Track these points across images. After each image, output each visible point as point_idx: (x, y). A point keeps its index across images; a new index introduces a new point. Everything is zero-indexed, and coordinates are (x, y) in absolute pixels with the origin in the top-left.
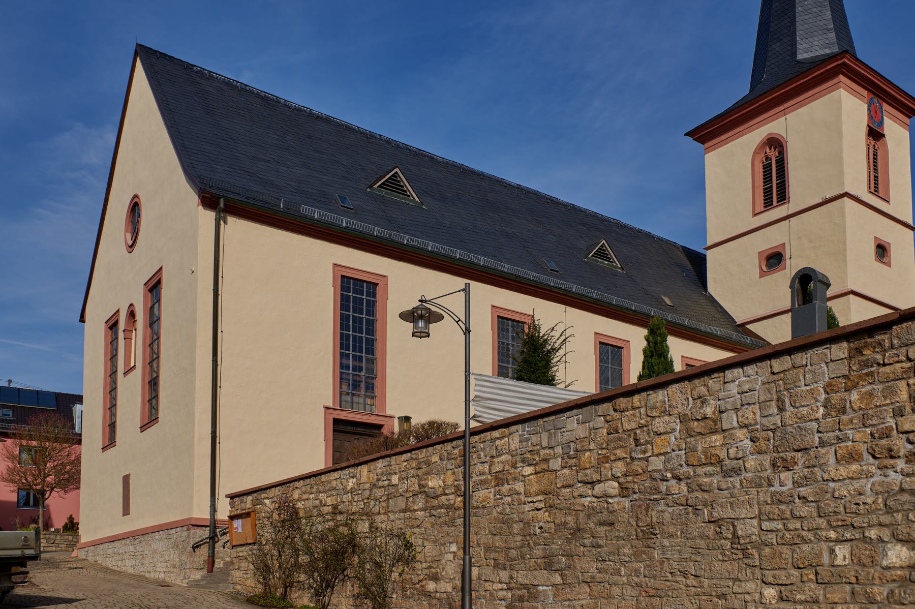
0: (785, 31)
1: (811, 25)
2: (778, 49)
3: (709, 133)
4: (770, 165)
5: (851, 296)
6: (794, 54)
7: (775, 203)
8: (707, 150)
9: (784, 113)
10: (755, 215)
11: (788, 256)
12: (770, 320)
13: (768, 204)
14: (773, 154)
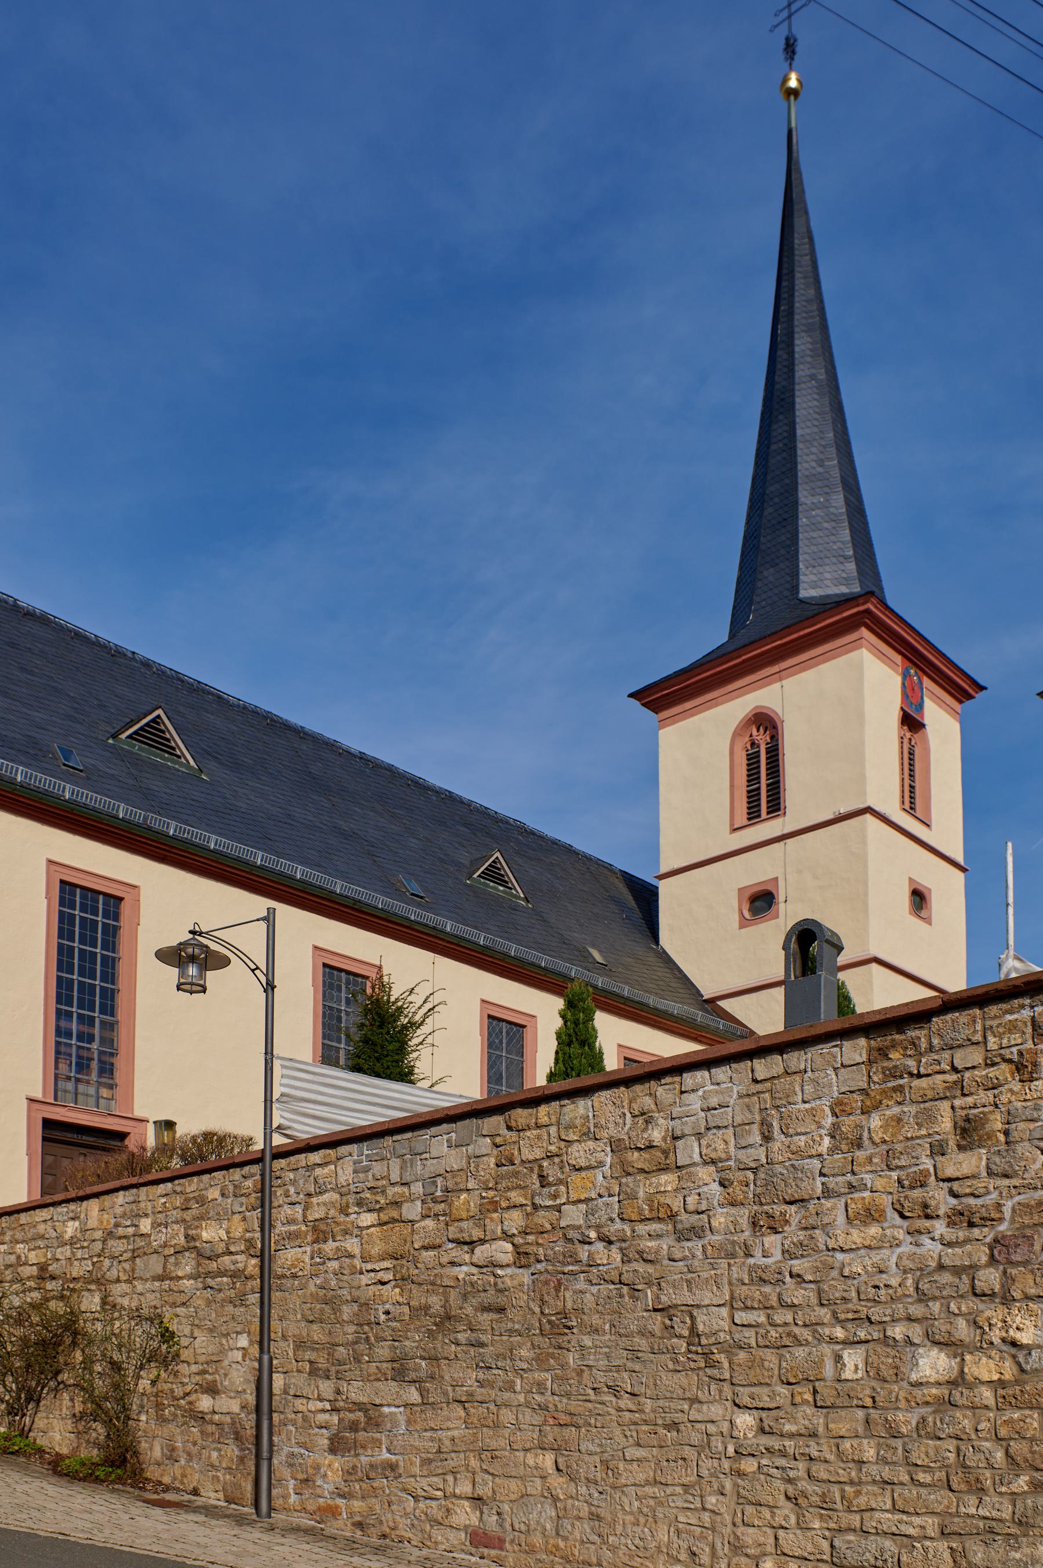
0: (783, 552)
2: (771, 578)
3: (665, 696)
4: (757, 755)
5: (874, 966)
6: (795, 588)
7: (764, 815)
8: (663, 723)
9: (779, 676)
10: (734, 830)
11: (781, 898)
13: (754, 815)
14: (763, 739)
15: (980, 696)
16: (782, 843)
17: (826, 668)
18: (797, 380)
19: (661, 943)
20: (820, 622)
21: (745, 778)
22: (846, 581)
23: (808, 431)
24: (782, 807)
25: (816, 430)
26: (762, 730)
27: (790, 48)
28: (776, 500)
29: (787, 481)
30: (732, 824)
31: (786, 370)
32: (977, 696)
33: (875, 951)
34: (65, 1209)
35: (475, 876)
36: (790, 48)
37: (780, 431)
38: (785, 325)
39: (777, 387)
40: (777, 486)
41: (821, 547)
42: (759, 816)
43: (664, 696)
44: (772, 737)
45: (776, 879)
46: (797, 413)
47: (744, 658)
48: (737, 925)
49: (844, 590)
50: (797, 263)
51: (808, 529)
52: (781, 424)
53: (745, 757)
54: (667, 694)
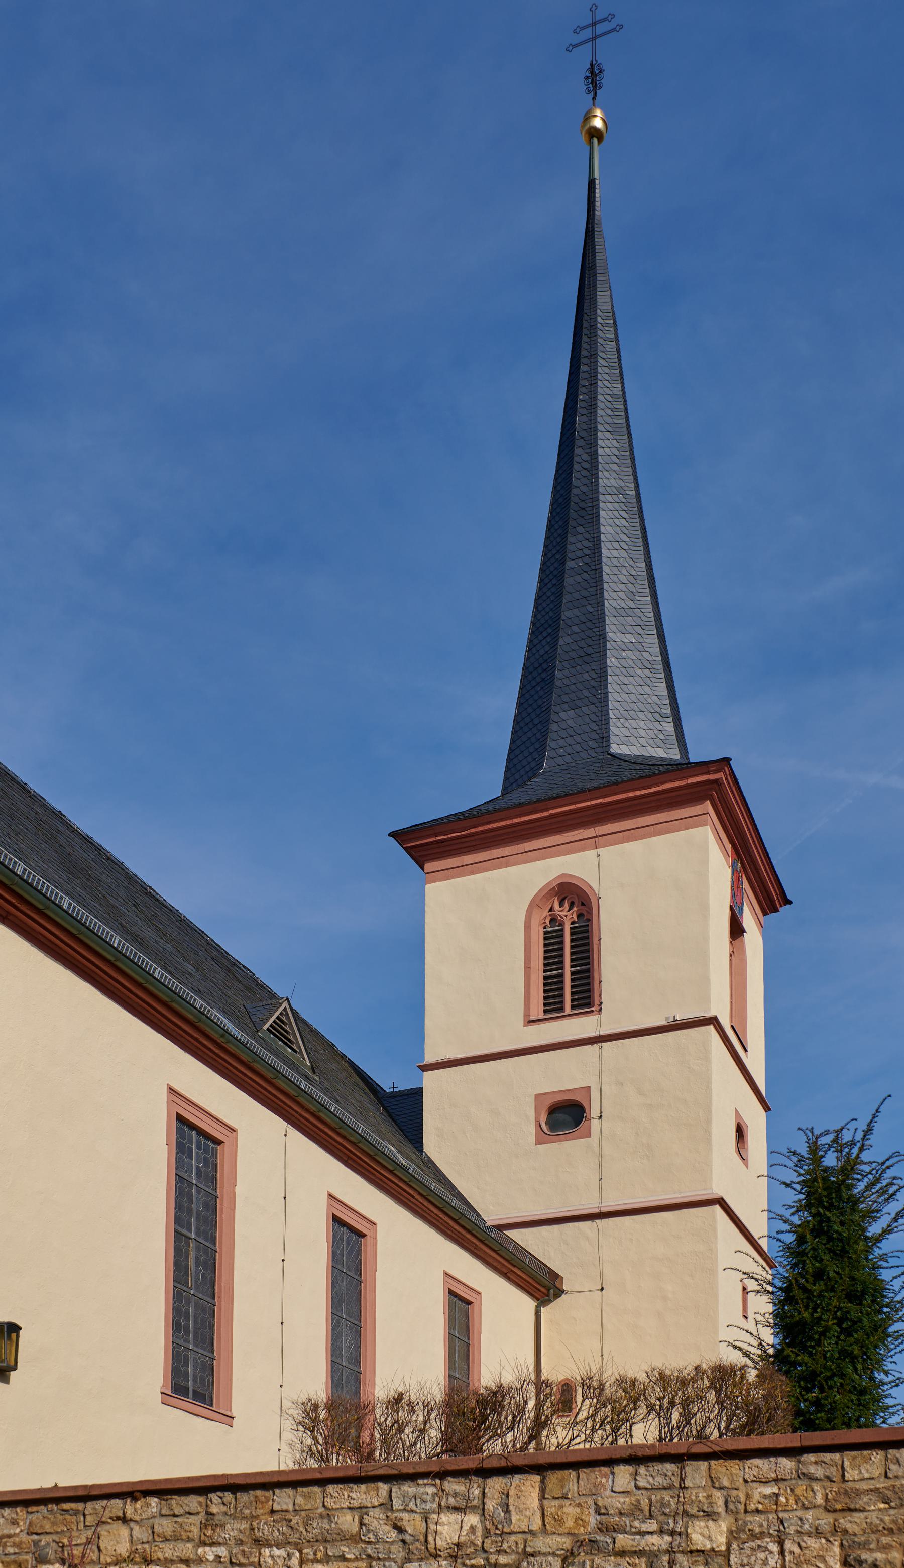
0: (586, 693)
1: (633, 697)
2: (571, 723)
3: (434, 843)
4: (560, 934)
5: (717, 1208)
6: (605, 740)
7: (568, 1010)
8: (436, 876)
9: (595, 842)
10: (531, 1022)
11: (595, 1113)
12: (556, 1228)
13: (553, 1006)
14: (568, 916)
15: (785, 909)
16: (596, 1047)
17: (658, 842)
18: (601, 490)
19: (426, 1149)
20: (657, 785)
21: (542, 962)
22: (664, 744)
23: (615, 553)
24: (597, 1002)
25: (625, 555)
26: (566, 905)
27: (594, 78)
28: (576, 629)
29: (590, 608)
30: (527, 1013)
31: (585, 473)
32: (780, 909)
33: (718, 1191)
34: (431, 1490)
35: (265, 1028)
36: (594, 78)
37: (579, 546)
38: (585, 419)
39: (575, 491)
40: (576, 612)
41: (633, 697)
42: (562, 1009)
43: (437, 842)
44: (580, 916)
45: (588, 1089)
46: (602, 529)
47: (551, 812)
48: (532, 1139)
49: (661, 753)
50: (600, 348)
51: (617, 671)
52: (580, 537)
53: (542, 934)
54: (442, 841)
